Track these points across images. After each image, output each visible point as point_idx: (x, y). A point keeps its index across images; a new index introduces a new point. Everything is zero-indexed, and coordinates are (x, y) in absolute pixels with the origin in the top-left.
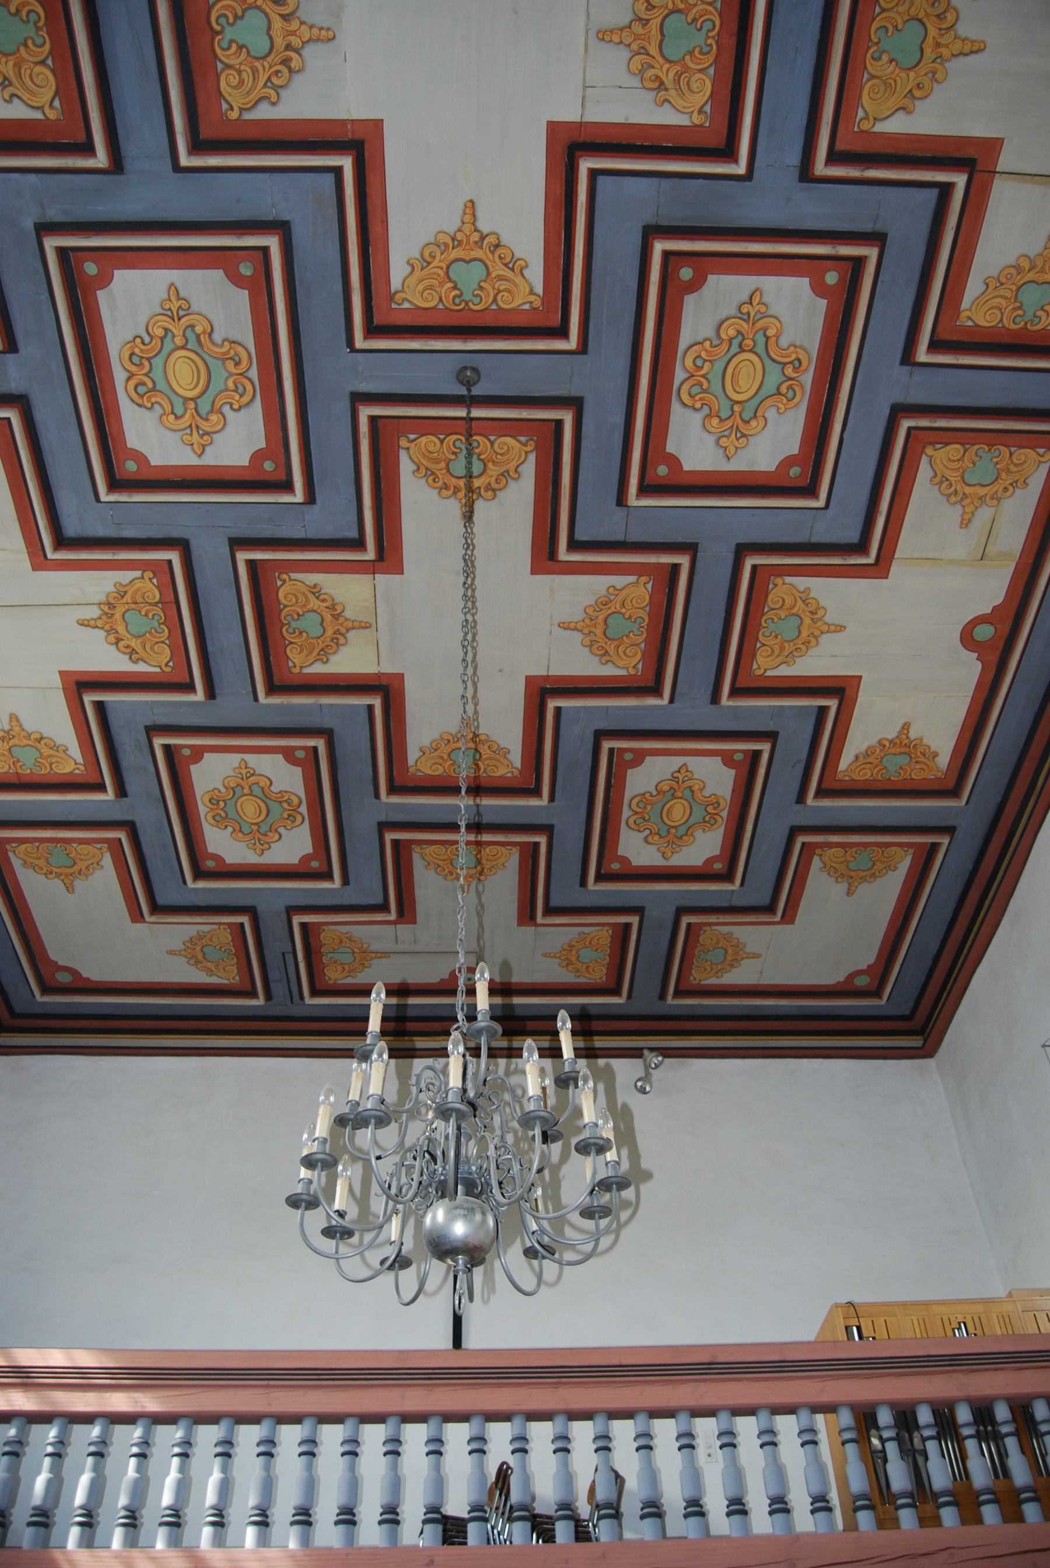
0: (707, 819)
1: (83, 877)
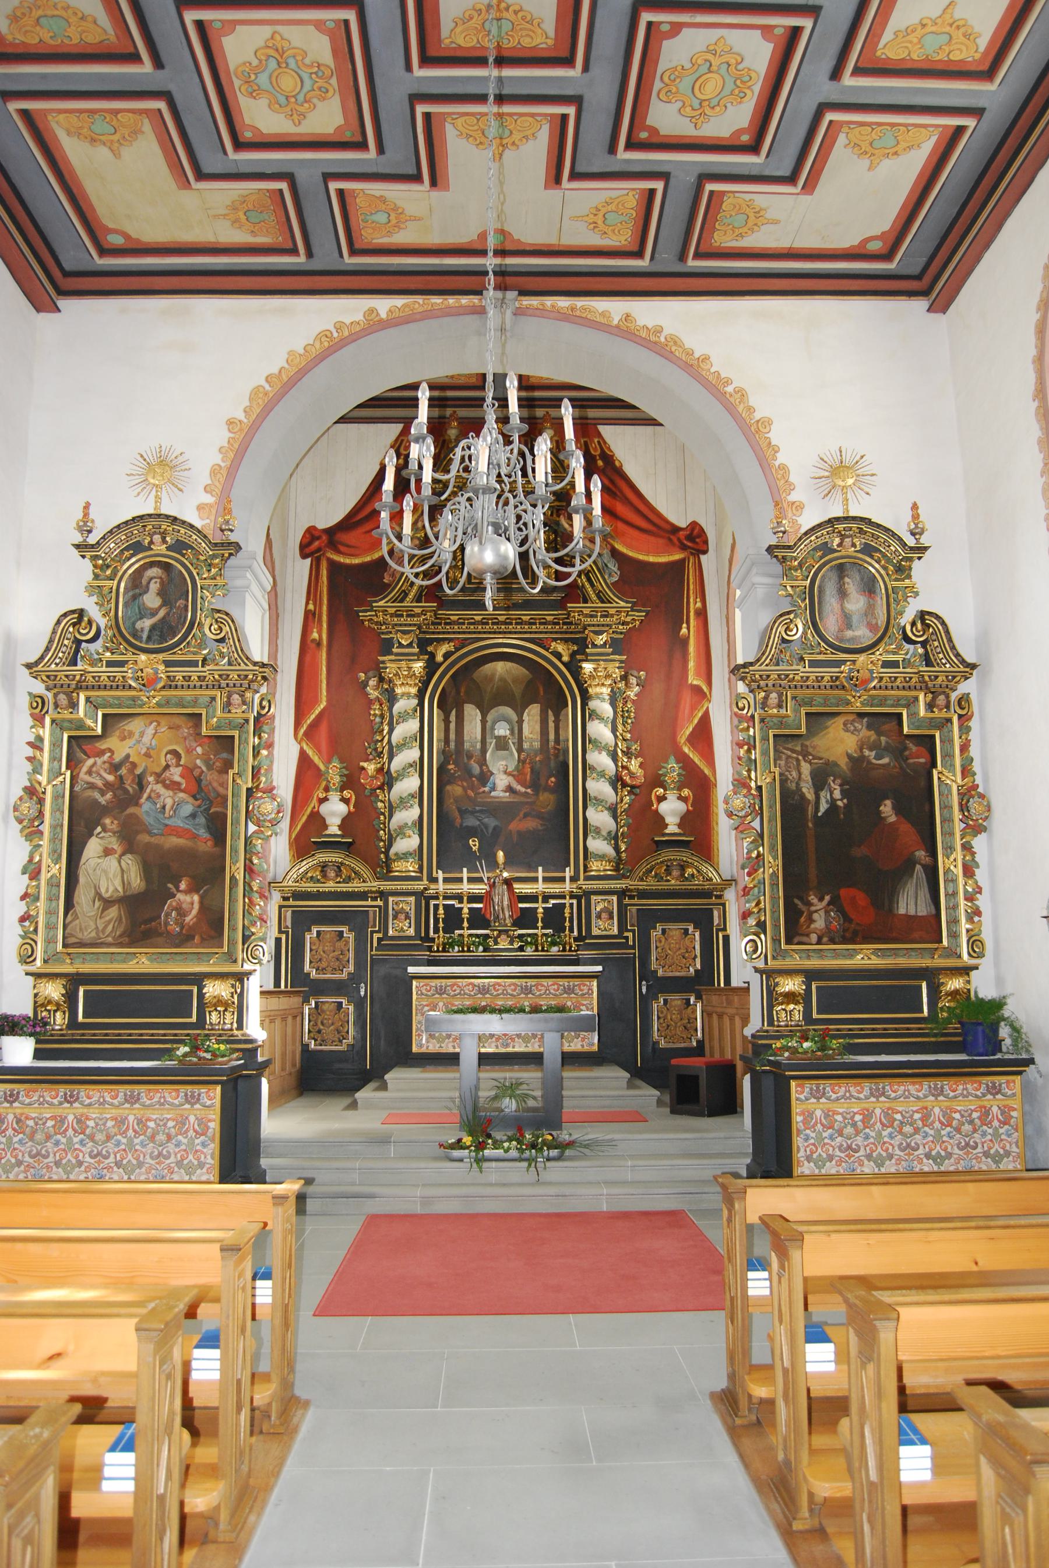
0: (737, 92)
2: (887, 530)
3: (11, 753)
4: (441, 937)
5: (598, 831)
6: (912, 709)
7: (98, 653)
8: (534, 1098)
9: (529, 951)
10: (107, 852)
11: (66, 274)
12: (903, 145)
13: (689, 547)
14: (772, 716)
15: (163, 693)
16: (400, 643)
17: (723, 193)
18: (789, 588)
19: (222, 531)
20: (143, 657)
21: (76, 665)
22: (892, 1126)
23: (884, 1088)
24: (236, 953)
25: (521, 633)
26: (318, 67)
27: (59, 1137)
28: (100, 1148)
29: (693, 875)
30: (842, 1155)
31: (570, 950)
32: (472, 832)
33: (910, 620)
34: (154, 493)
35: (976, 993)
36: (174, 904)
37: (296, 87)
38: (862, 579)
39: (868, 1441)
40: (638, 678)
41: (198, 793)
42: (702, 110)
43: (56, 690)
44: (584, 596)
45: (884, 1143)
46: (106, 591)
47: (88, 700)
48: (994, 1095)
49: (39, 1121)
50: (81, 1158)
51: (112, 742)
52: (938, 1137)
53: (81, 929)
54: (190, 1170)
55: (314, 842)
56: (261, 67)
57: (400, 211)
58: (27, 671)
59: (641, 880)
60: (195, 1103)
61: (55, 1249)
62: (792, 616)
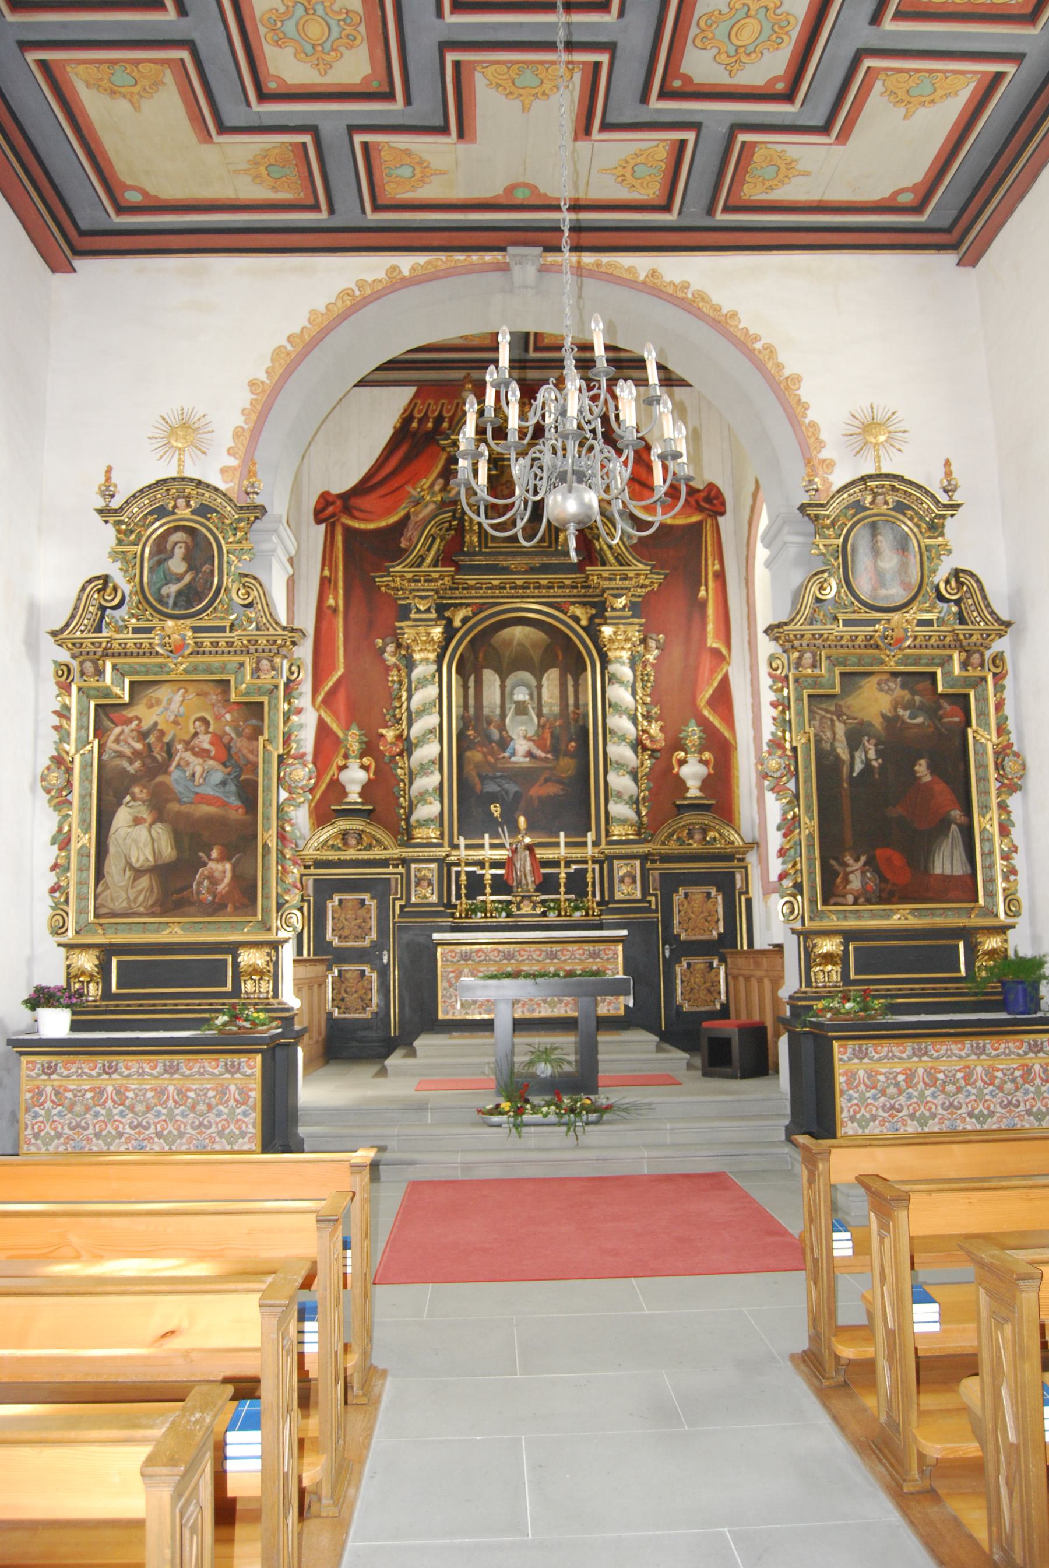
0: (774, 37)
2: (919, 487)
3: (37, 723)
4: (465, 903)
5: (619, 795)
6: (947, 668)
7: (124, 620)
8: (569, 1063)
9: (552, 916)
10: (137, 821)
11: (82, 233)
12: (940, 92)
13: (707, 509)
14: (807, 676)
15: (190, 659)
16: (418, 609)
17: (755, 143)
18: (821, 547)
19: (248, 494)
20: (170, 623)
21: (101, 632)
22: (934, 1085)
23: (926, 1048)
24: (271, 921)
25: (539, 597)
26: (347, 13)
27: (98, 1108)
28: (140, 1119)
29: (715, 839)
30: (886, 1115)
31: (593, 915)
32: (493, 798)
33: (944, 578)
34: (176, 456)
35: (1016, 951)
36: (206, 872)
37: (323, 34)
38: (895, 538)
39: (1006, 1401)
40: (657, 641)
41: (228, 760)
42: (738, 57)
43: (82, 658)
44: (602, 557)
45: (927, 1102)
46: (130, 556)
47: (114, 667)
48: (1036, 1053)
49: (79, 1093)
50: (121, 1129)
51: (139, 710)
52: (980, 1096)
53: (112, 900)
54: (231, 1139)
55: (334, 810)
56: (288, 14)
57: (425, 164)
58: (51, 639)
59: (663, 843)
60: (236, 1073)
61: (141, 1223)
62: (826, 575)
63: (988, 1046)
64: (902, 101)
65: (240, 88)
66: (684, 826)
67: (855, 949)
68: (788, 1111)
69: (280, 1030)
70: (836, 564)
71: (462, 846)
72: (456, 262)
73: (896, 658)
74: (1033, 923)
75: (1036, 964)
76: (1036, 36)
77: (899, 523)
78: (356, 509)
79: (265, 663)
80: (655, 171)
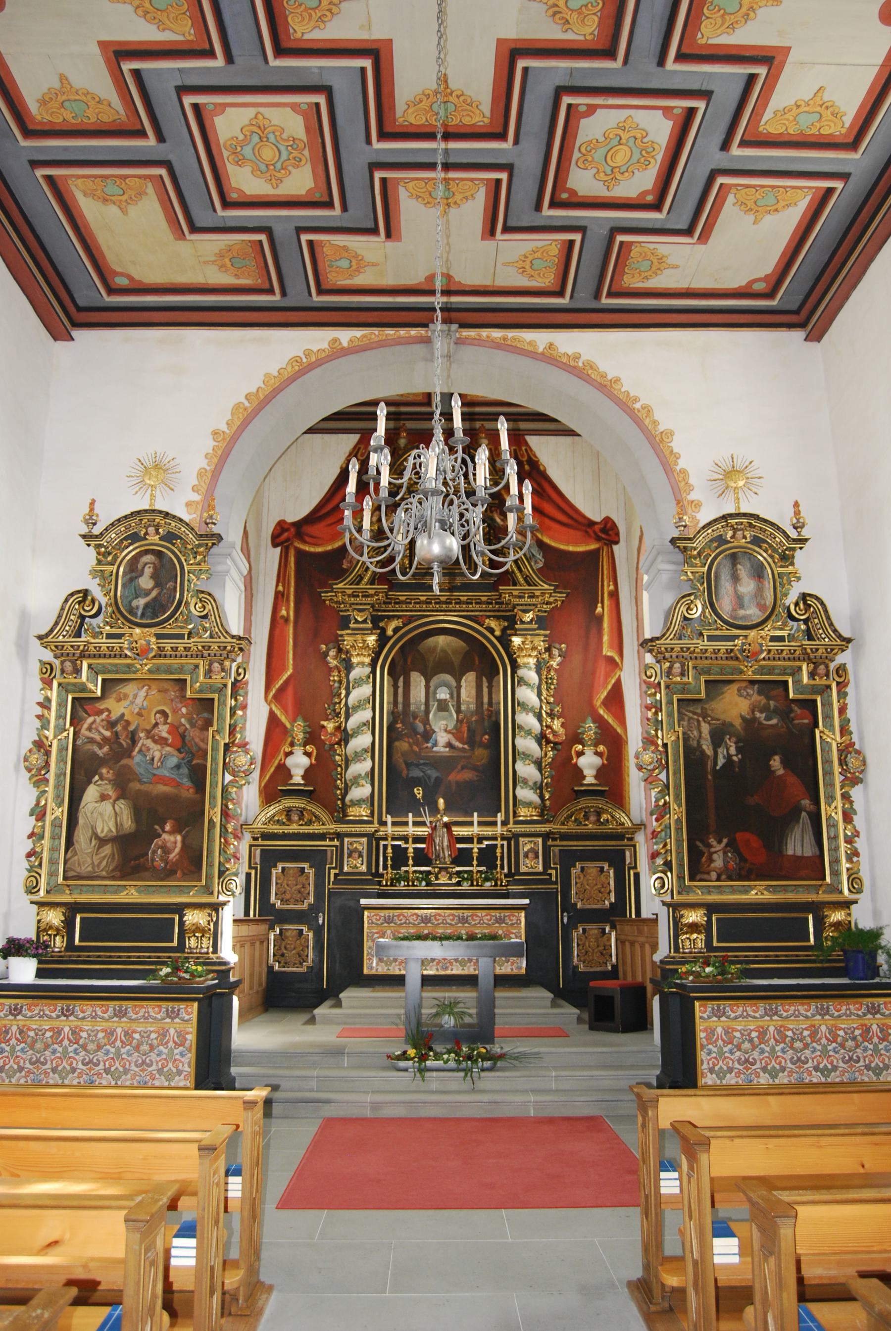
1: (53, 91)
3: (23, 712)
4: (390, 873)
5: (525, 782)
6: (797, 677)
7: (99, 627)
8: (470, 1015)
9: (466, 886)
10: (103, 797)
11: (80, 309)
12: (782, 203)
13: (603, 539)
14: (676, 683)
15: (153, 661)
16: (356, 619)
17: (632, 243)
18: (689, 574)
19: (207, 524)
20: (138, 631)
21: (80, 637)
23: (776, 1008)
25: (459, 611)
27: (56, 1046)
28: (91, 1057)
29: (607, 820)
30: (741, 1067)
31: (501, 885)
32: (417, 782)
33: (794, 601)
34: (149, 490)
35: (856, 924)
36: (160, 843)
37: (275, 157)
38: (752, 566)
40: (560, 650)
42: (613, 175)
43: (63, 658)
45: (778, 1057)
46: (107, 574)
48: (874, 1014)
50: (74, 1065)
52: (824, 1052)
53: (79, 864)
54: (169, 1077)
55: (281, 790)
56: (246, 140)
57: (360, 258)
58: (38, 642)
59: (563, 824)
60: (175, 1018)
62: (692, 598)
63: (831, 1008)
64: (751, 210)
65: (208, 197)
66: (581, 809)
67: (717, 919)
68: (660, 1063)
69: (216, 981)
70: (701, 589)
71: (389, 823)
72: (386, 335)
73: (753, 669)
74: (874, 899)
75: (875, 935)
76: (858, 160)
77: (755, 554)
78: (307, 535)
79: (216, 666)
80: (550, 264)
